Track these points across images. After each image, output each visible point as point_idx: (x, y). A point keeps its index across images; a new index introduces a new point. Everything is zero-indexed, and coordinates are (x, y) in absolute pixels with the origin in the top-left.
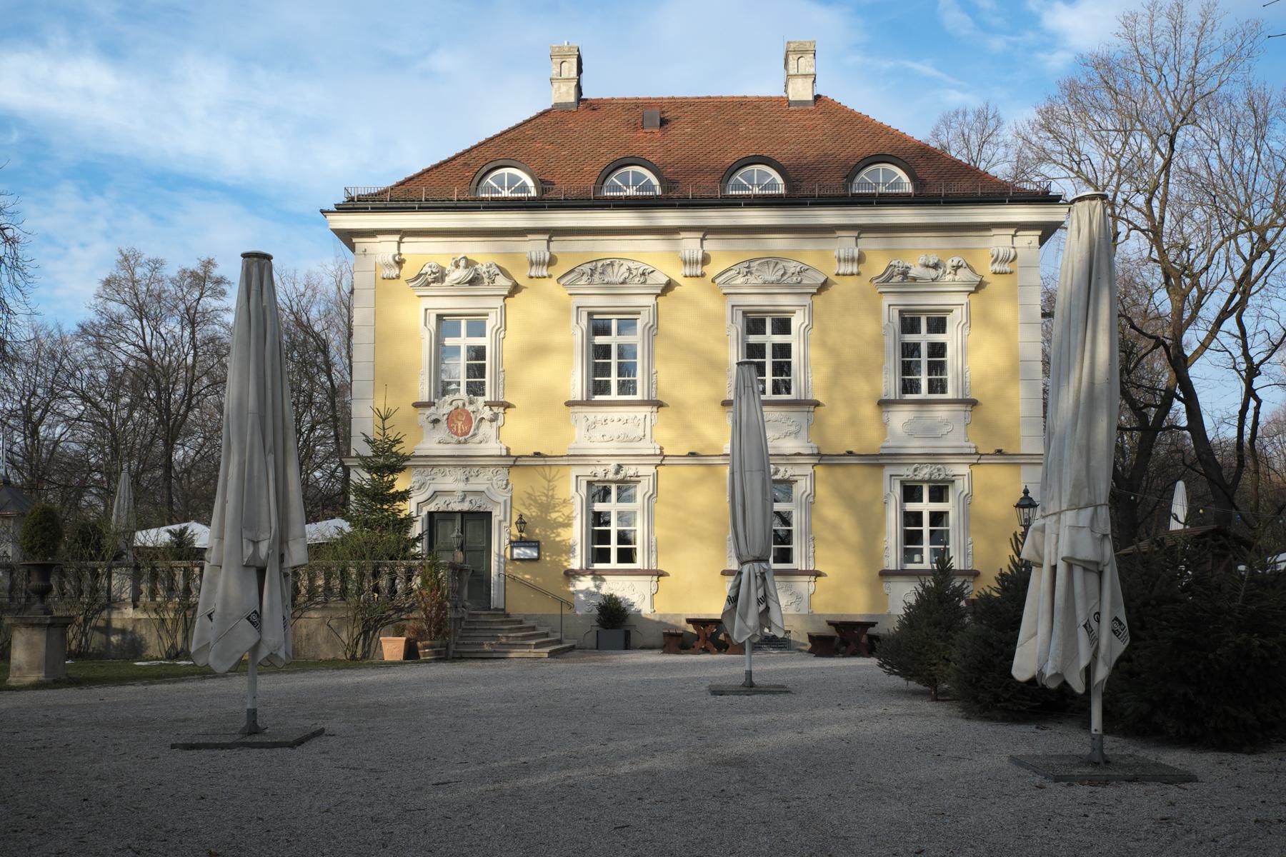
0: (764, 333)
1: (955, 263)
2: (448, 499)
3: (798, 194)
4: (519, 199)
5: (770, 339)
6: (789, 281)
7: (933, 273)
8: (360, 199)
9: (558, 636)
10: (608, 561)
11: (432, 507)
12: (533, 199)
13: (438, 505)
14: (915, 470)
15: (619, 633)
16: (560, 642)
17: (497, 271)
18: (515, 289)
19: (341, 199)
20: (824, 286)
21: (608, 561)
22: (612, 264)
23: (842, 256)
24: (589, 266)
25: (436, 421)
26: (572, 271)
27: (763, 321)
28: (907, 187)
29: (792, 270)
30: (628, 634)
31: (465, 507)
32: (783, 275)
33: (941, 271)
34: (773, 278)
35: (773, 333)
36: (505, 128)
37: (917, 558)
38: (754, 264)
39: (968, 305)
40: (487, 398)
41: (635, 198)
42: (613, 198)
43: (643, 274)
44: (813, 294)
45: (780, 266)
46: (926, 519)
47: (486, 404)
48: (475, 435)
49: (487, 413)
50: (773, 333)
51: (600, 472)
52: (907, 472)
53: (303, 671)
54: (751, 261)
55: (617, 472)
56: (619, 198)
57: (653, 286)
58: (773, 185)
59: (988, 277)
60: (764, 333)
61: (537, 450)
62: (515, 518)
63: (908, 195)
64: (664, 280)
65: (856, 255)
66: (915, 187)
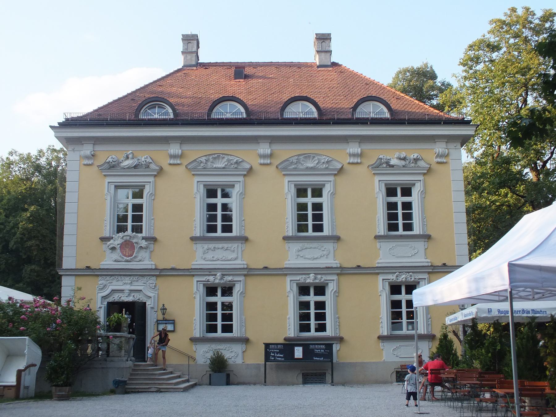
0: (307, 197)
1: (415, 157)
2: (121, 295)
3: (324, 118)
4: (164, 120)
5: (399, 199)
6: (321, 167)
7: (403, 163)
8: (73, 119)
9: (186, 378)
10: (216, 232)
11: (111, 299)
12: (172, 119)
13: (116, 298)
14: (397, 276)
15: (223, 376)
16: (188, 381)
17: (151, 161)
18: (161, 171)
19: (62, 120)
20: (341, 171)
21: (216, 232)
22: (219, 156)
23: (351, 153)
24: (204, 158)
25: (113, 249)
26: (195, 160)
27: (395, 189)
28: (387, 115)
29: (323, 161)
30: (228, 376)
31: (130, 299)
32: (317, 164)
33: (407, 162)
34: (223, 166)
35: (402, 196)
36: (155, 79)
37: (410, 327)
38: (301, 157)
39: (424, 180)
40: (144, 234)
41: (231, 119)
42: (218, 119)
43: (236, 163)
44: (335, 175)
45: (316, 158)
46: (219, 307)
47: (143, 238)
48: (135, 257)
49: (144, 243)
50: (402, 196)
51: (211, 278)
52: (301, 279)
53: (95, 398)
54: (299, 155)
55: (221, 279)
56: (151, 120)
57: (244, 169)
58: (381, 112)
59: (256, 166)
60: (307, 197)
61: (359, 265)
62: (161, 306)
63: (388, 119)
64: (248, 166)
65: (359, 152)
66: (391, 115)
